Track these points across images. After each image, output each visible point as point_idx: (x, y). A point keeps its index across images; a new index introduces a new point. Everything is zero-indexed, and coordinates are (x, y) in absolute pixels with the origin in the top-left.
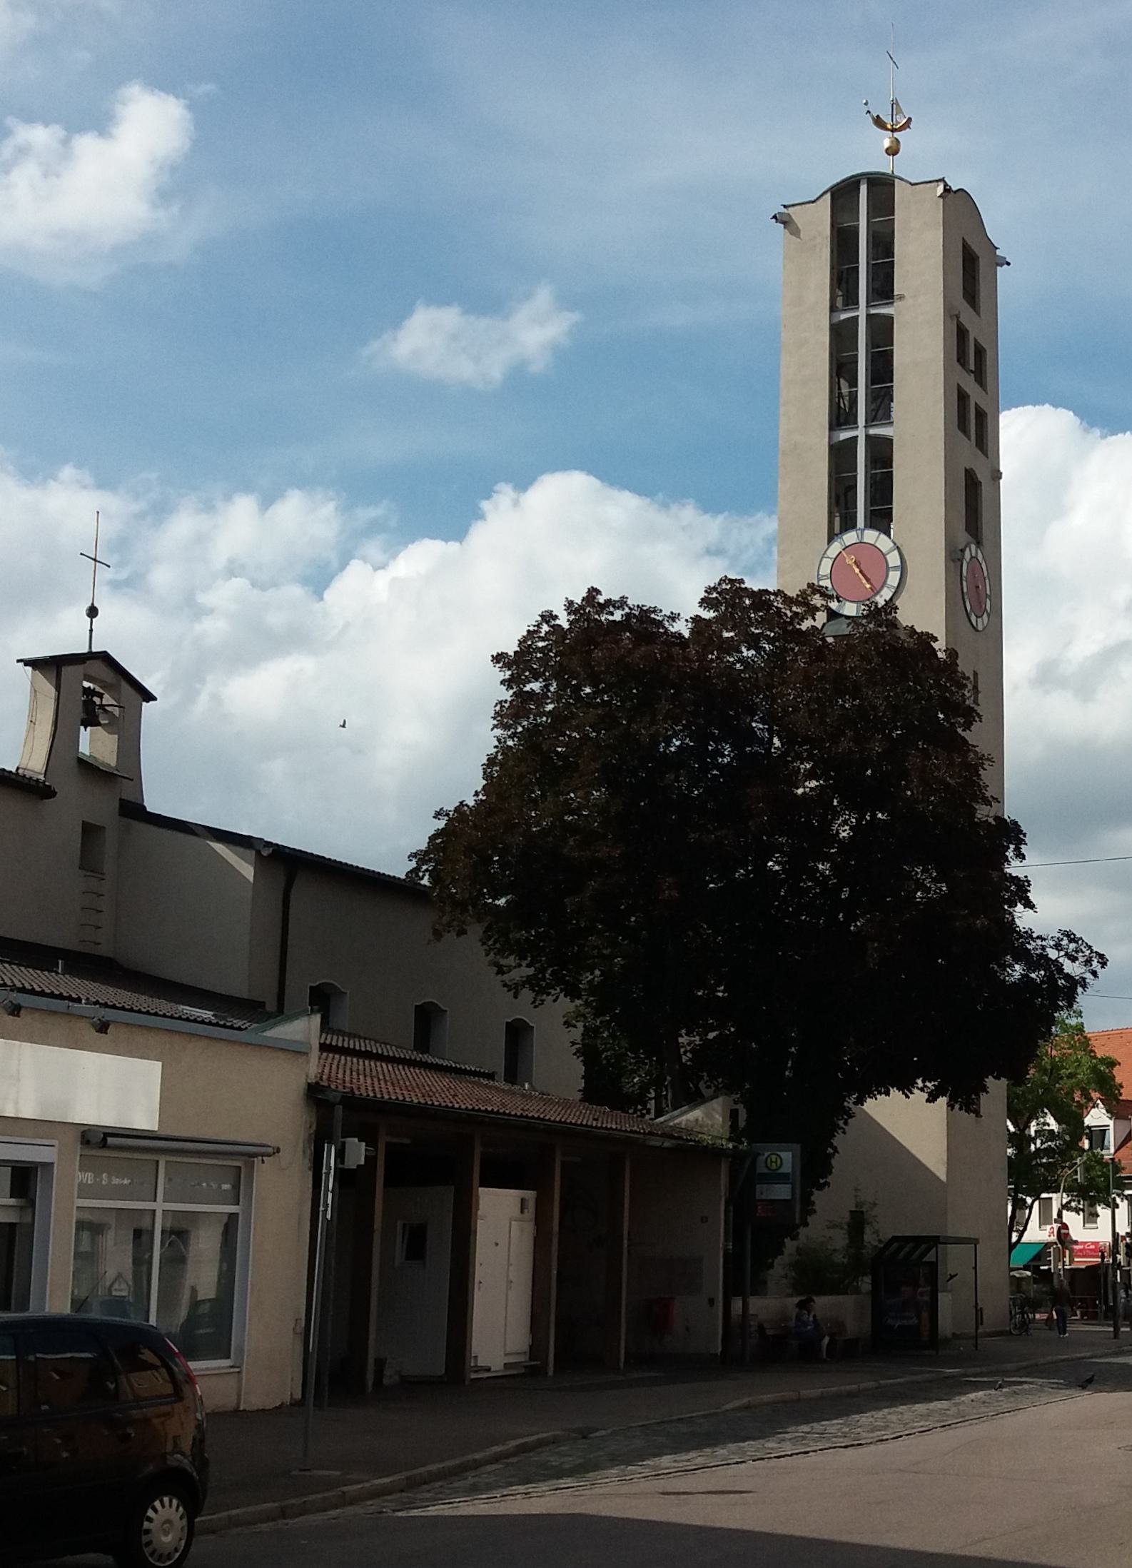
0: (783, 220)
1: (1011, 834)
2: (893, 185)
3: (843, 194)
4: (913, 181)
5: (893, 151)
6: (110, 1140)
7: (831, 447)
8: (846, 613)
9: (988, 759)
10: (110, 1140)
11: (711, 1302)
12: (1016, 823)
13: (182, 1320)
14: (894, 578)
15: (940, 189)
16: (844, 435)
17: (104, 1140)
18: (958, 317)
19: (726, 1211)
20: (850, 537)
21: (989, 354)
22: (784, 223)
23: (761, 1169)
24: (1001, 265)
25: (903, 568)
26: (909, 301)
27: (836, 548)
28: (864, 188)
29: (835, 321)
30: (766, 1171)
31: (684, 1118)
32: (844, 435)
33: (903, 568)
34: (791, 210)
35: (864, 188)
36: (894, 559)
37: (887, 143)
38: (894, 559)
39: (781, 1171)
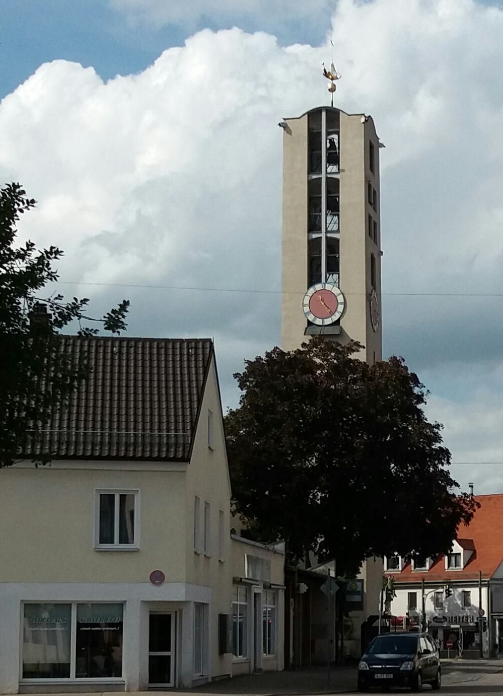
0: (284, 126)
1: (445, 454)
2: (339, 114)
3: (314, 115)
4: (349, 114)
5: (332, 90)
6: (272, 586)
7: (309, 242)
8: (317, 323)
9: (442, 426)
10: (272, 586)
11: (332, 642)
12: (447, 449)
13: (232, 645)
14: (340, 308)
15: (363, 120)
16: (315, 236)
17: (270, 587)
18: (369, 181)
19: (336, 607)
20: (318, 287)
21: (377, 192)
22: (284, 127)
23: (348, 589)
24: (381, 147)
25: (345, 303)
26: (347, 173)
27: (312, 290)
28: (324, 114)
29: (310, 179)
30: (350, 590)
31: (318, 569)
32: (315, 236)
33: (345, 303)
34: (287, 121)
35: (324, 114)
36: (340, 299)
37: (330, 86)
38: (340, 299)
39: (357, 590)
